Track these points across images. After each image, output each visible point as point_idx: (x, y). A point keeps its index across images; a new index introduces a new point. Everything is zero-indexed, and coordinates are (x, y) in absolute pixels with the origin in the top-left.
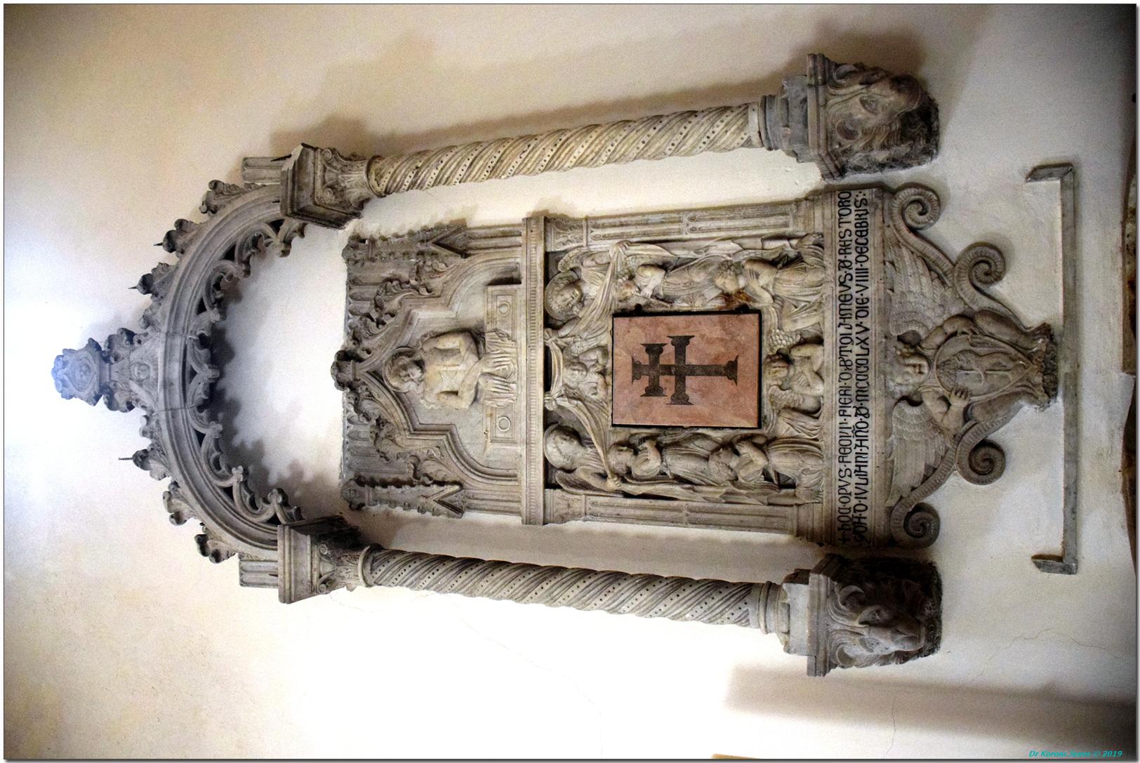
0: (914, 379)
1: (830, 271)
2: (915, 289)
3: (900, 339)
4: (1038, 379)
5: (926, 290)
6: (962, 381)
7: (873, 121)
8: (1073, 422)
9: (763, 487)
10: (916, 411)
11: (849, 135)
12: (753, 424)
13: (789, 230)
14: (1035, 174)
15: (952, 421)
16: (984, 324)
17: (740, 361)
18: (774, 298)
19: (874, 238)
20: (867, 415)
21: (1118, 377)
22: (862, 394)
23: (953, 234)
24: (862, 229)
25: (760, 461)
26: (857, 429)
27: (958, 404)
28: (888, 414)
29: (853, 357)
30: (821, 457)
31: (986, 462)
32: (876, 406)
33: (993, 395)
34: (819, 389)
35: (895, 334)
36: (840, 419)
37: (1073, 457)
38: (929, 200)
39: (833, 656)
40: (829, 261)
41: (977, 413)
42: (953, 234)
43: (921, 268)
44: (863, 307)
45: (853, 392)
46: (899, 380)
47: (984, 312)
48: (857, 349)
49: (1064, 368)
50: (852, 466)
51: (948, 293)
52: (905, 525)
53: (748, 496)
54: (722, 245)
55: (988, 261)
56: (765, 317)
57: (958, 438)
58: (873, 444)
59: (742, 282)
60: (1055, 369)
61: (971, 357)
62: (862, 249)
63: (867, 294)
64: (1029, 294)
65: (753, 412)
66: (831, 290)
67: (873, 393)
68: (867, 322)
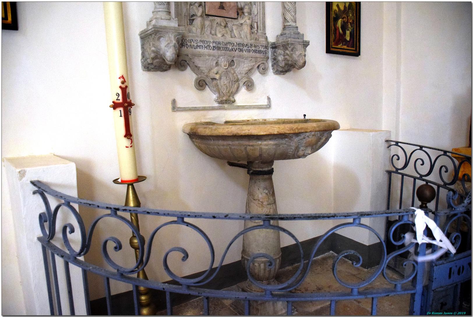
0: (223, 64)
1: (250, 42)
2: (245, 66)
3: (233, 61)
4: (224, 99)
5: (245, 69)
6: (224, 78)
7: (294, 56)
8: (213, 109)
9: (190, 14)
10: (214, 64)
11: (292, 50)
12: (206, 13)
13: (259, 31)
14: (269, 99)
15: (212, 75)
16: (235, 85)
17: (224, 11)
18: (242, 24)
19: (258, 55)
20: (213, 50)
21: (224, 120)
22: (219, 49)
23: (256, 77)
24: (260, 52)
25: (199, 14)
26: (209, 46)
27: (217, 77)
28: (214, 56)
29: (228, 46)
30: (201, 34)
31: (201, 85)
32: (216, 52)
33: (220, 87)
34: (219, 35)
35: (234, 59)
36: (212, 41)
37: (204, 109)
38: (264, 71)
39: (160, 34)
40: (253, 41)
41: (215, 82)
42: (256, 77)
43: (250, 68)
44: (241, 50)
45: (219, 46)
46: (223, 60)
47: (239, 84)
48: (230, 48)
49: (226, 106)
50: (199, 44)
51: (243, 75)
52: (183, 60)
53: (187, 9)
54: (256, 9)
55: (250, 86)
56: (236, 20)
57: (207, 76)
58: (205, 51)
59: (246, 14)
60: (226, 103)
61: (229, 81)
62: (255, 51)
63: (244, 52)
64: (242, 97)
65: (210, 13)
66: (245, 42)
67: (219, 52)
68: (237, 51)
